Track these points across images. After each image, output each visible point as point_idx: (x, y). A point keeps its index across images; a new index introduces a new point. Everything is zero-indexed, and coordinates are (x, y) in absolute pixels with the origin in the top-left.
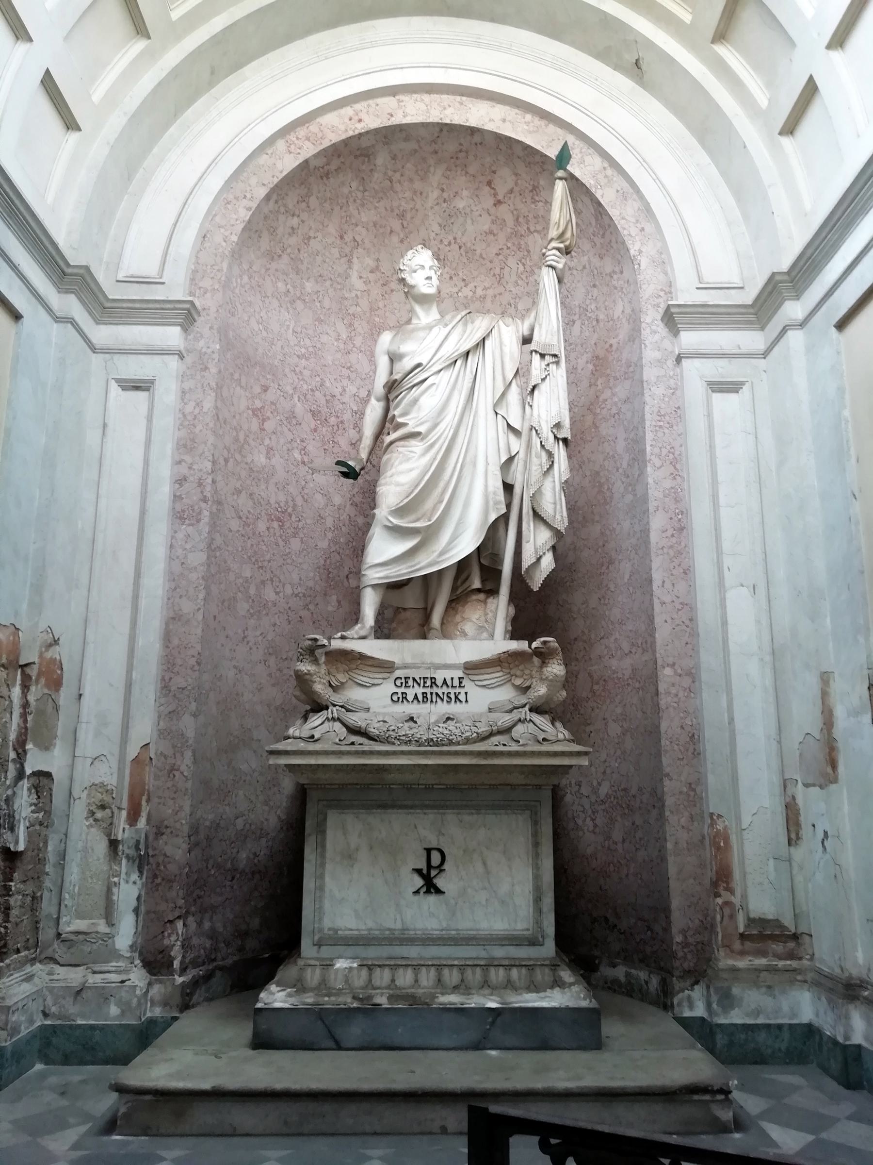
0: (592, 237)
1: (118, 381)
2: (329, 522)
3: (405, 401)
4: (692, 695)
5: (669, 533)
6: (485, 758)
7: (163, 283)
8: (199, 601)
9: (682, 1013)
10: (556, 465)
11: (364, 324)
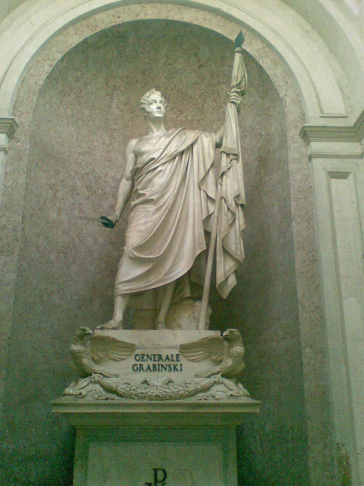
2: (96, 255)
10: (237, 221)
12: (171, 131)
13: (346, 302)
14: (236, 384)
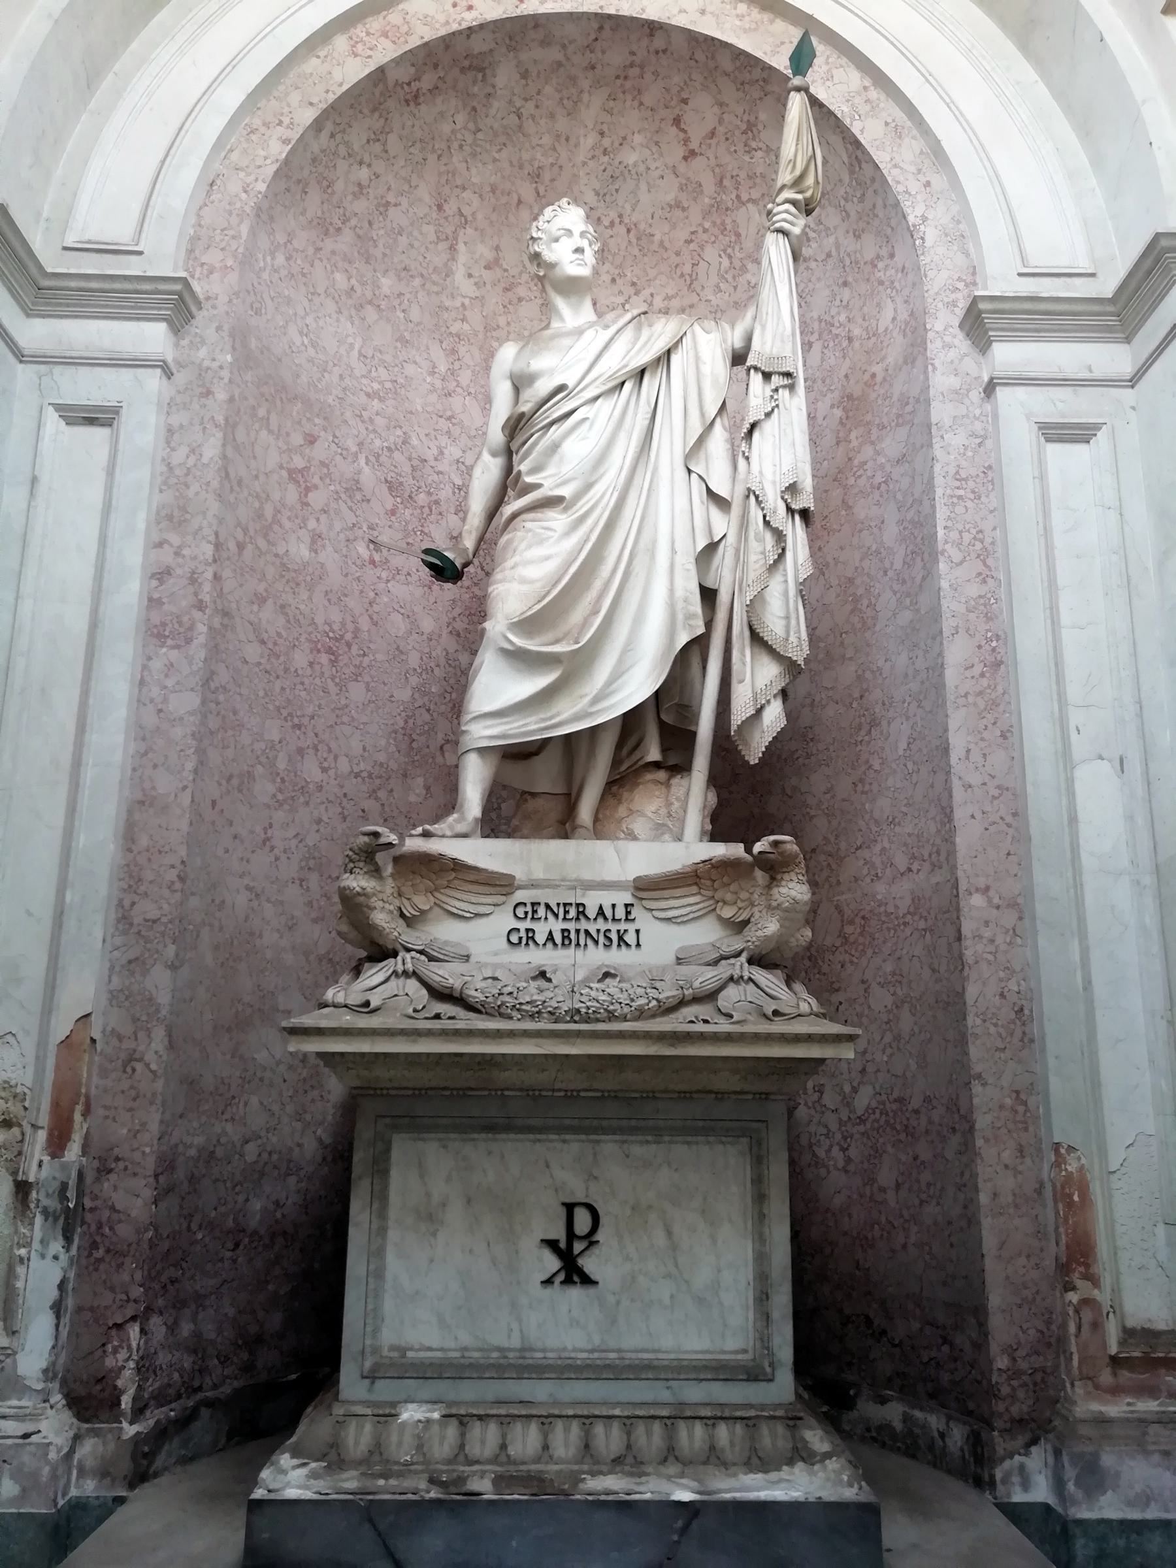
0: (843, 203)
1: (58, 407)
2: (414, 660)
3: (539, 448)
4: (1019, 940)
5: (977, 670)
6: (672, 1045)
7: (140, 253)
8: (185, 774)
9: (1009, 1495)
10: (789, 555)
11: (476, 353)
12: (610, 316)
13: (1083, 775)
14: (789, 982)
